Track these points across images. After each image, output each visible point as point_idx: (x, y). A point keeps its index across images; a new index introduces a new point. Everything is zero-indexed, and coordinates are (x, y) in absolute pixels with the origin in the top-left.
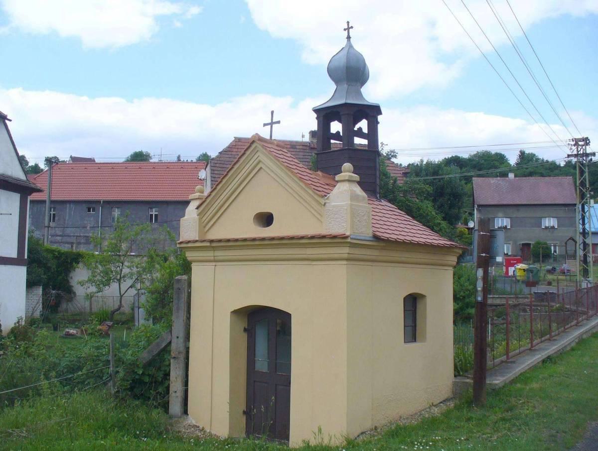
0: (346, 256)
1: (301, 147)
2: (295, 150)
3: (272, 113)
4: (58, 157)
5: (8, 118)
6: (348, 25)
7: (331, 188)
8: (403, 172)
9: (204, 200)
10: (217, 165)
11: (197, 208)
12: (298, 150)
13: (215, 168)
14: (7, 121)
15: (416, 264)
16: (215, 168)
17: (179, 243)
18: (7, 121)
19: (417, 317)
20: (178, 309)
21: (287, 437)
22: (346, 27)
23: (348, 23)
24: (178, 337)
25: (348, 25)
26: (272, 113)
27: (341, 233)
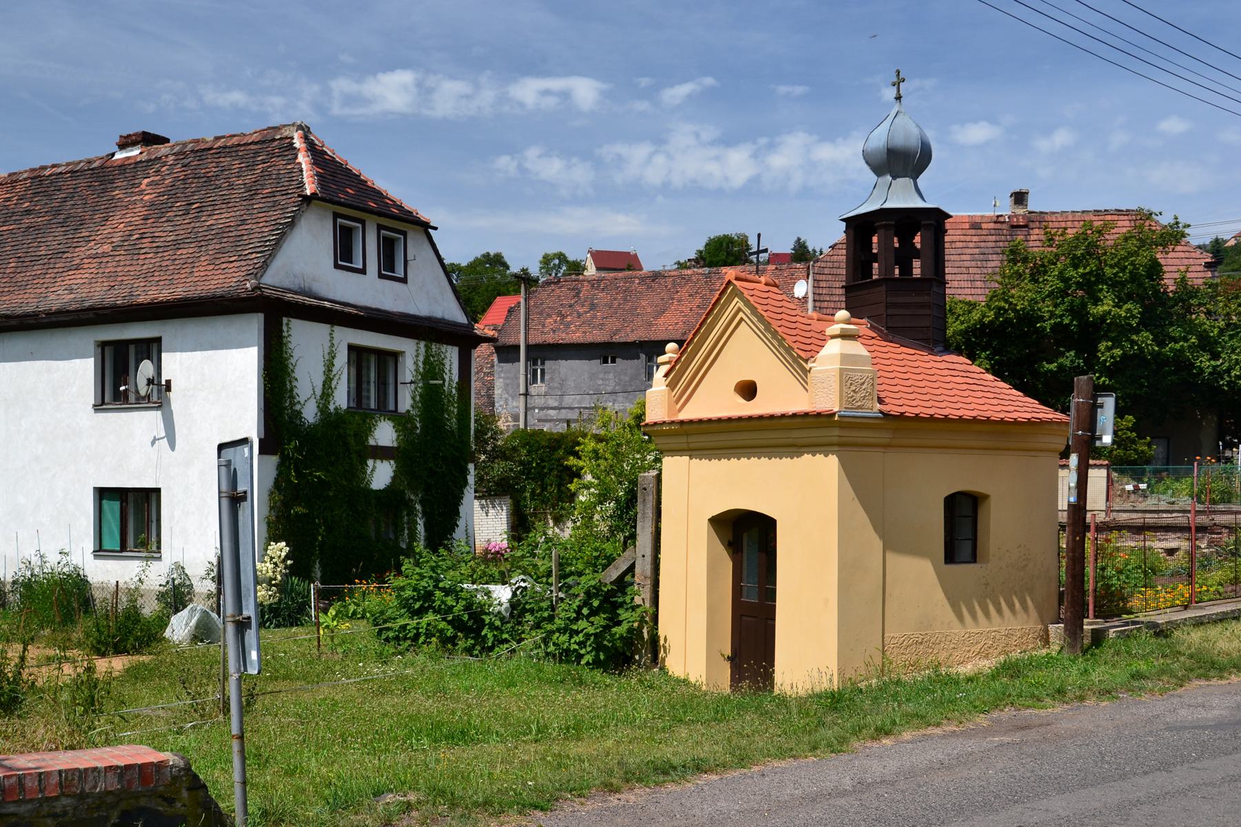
0: (835, 440)
1: (992, 226)
2: (979, 232)
3: (759, 235)
4: (564, 252)
5: (432, 224)
6: (898, 75)
7: (820, 343)
8: (1207, 260)
9: (673, 363)
10: (826, 271)
11: (665, 376)
12: (984, 232)
13: (821, 277)
14: (430, 230)
15: (936, 447)
16: (821, 277)
17: (644, 426)
18: (430, 230)
19: (979, 528)
20: (644, 517)
21: (768, 677)
22: (895, 80)
23: (898, 72)
24: (644, 556)
25: (898, 75)
26: (759, 235)
27: (827, 409)
